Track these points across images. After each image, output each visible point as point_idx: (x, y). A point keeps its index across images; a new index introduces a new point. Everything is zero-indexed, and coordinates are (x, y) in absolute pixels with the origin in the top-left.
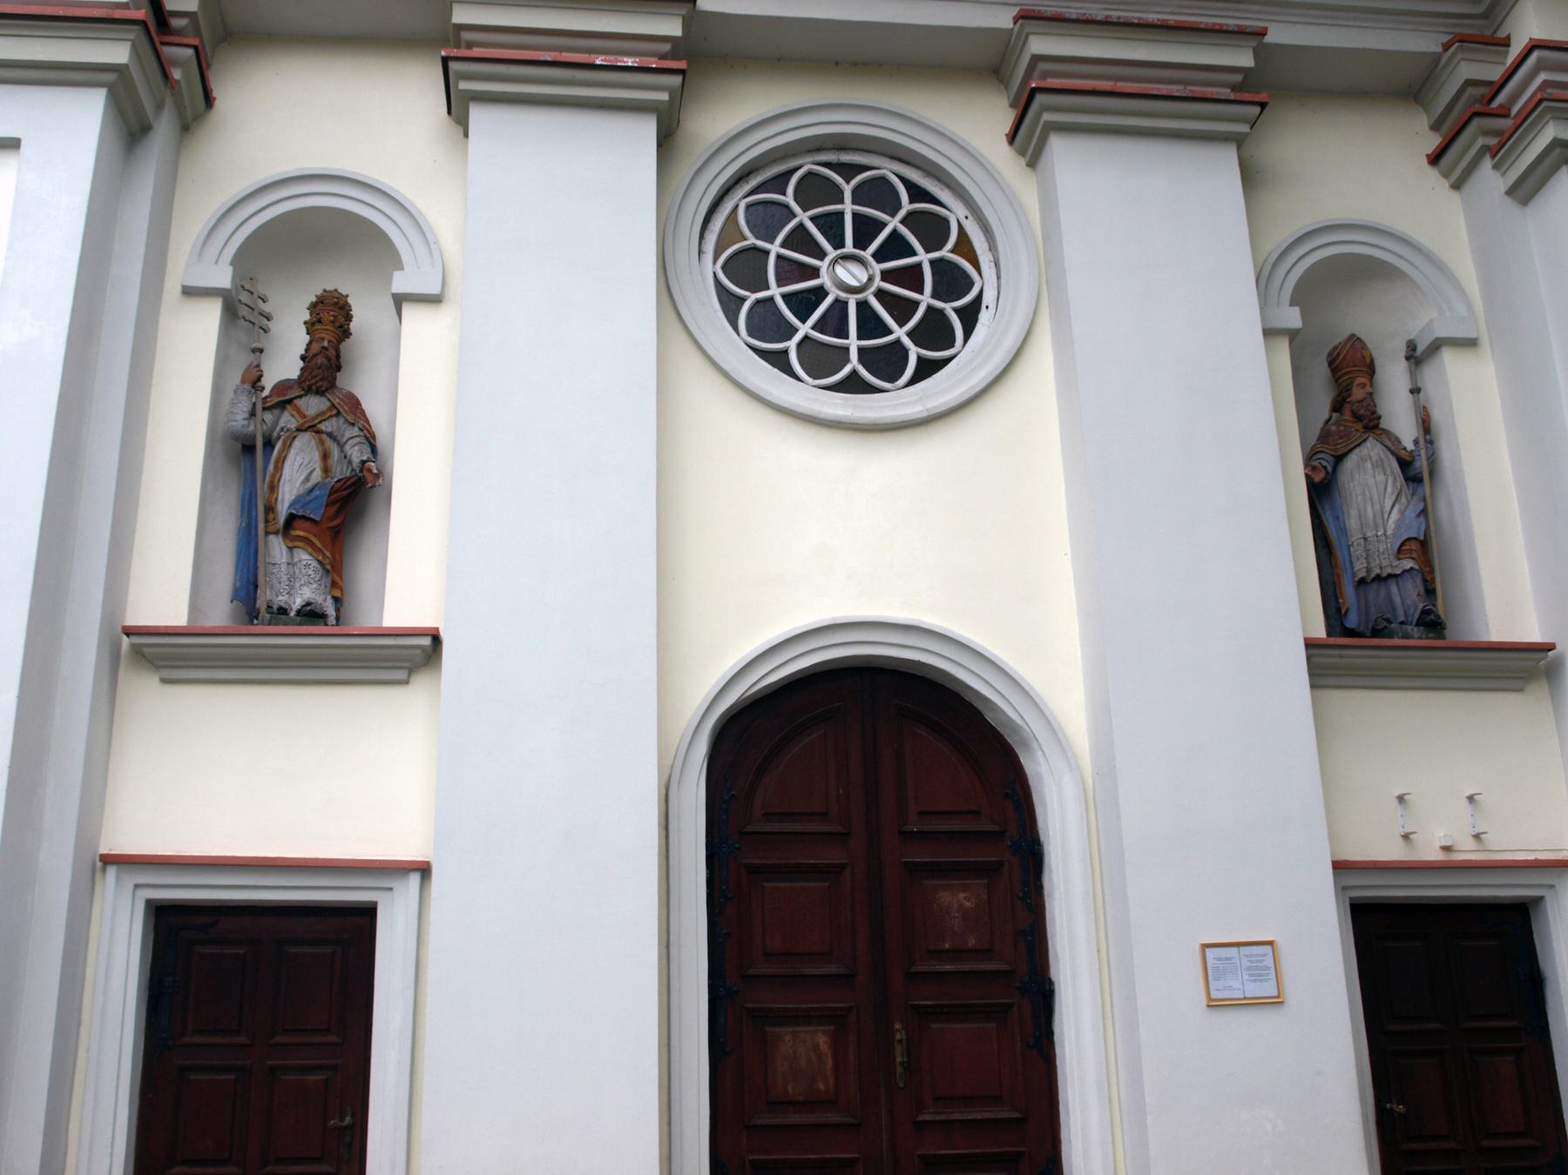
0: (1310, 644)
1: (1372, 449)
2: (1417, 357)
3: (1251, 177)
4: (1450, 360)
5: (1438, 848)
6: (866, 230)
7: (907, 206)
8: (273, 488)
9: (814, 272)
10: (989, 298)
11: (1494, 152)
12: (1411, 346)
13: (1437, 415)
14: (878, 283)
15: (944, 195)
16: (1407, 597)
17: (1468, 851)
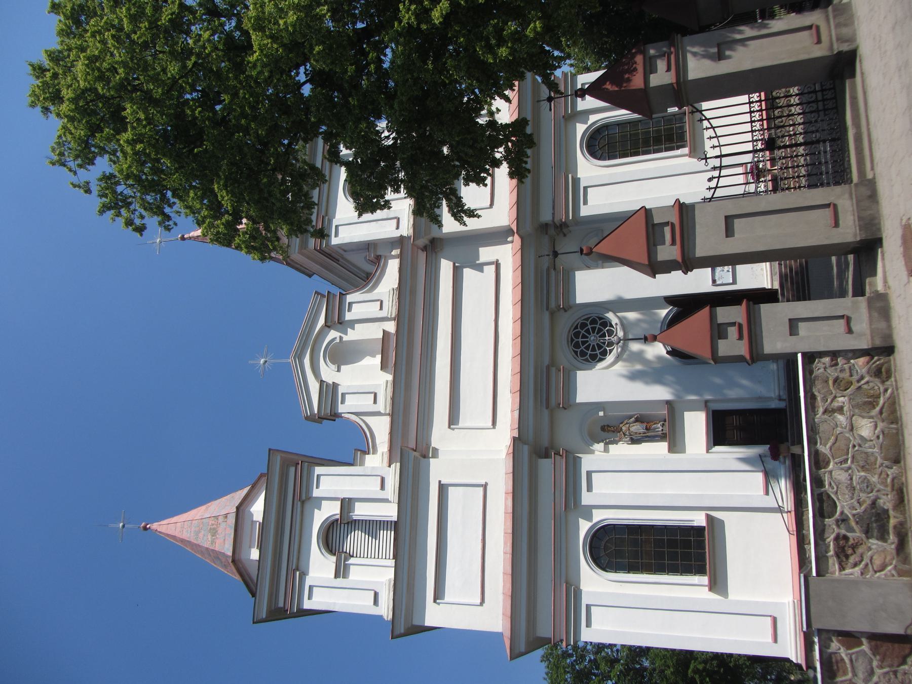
7: (579, 329)
10: (597, 315)
14: (590, 342)
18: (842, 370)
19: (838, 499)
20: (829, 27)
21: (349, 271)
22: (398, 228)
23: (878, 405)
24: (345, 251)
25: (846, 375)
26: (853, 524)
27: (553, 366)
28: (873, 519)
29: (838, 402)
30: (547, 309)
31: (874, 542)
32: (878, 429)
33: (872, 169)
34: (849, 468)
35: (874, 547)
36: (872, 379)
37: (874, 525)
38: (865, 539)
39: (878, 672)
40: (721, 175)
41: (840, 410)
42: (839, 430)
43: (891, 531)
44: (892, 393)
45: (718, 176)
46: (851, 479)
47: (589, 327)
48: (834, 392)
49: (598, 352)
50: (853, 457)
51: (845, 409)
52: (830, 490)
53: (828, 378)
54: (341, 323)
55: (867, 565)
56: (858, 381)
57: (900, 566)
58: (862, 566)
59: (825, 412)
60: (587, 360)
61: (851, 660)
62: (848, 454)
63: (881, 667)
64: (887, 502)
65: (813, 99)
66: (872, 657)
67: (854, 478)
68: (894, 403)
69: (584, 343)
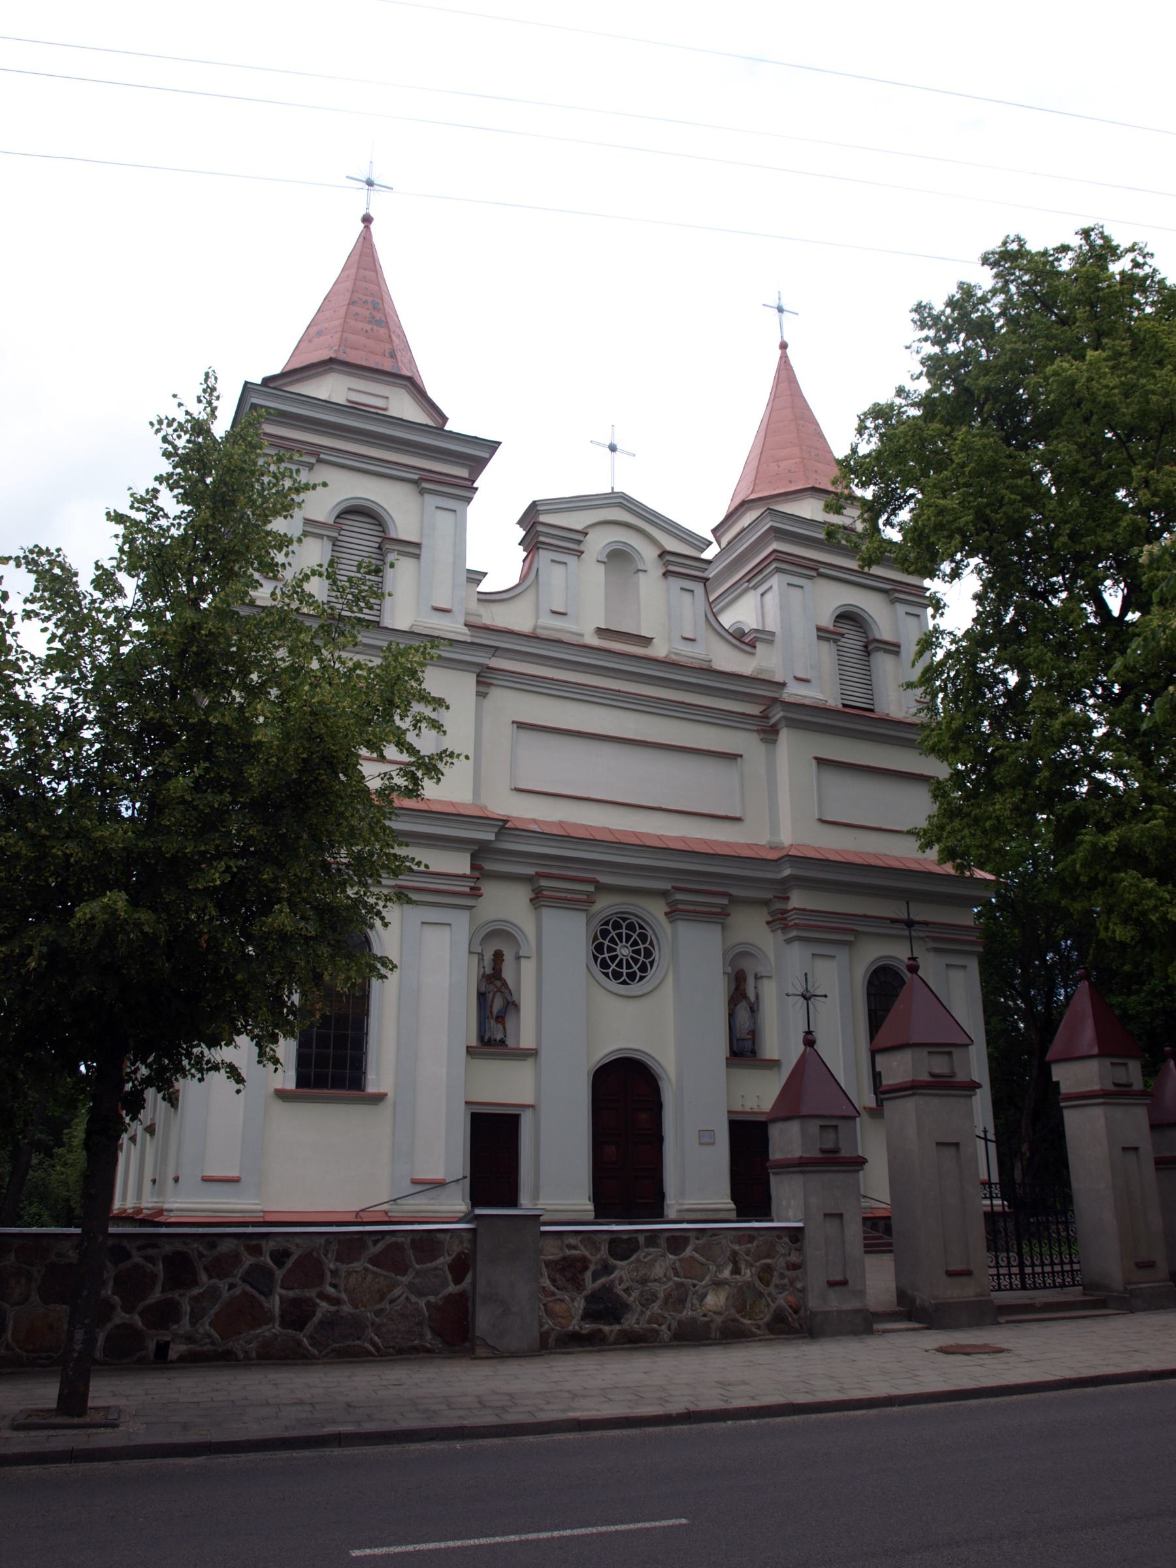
0: (727, 1058)
1: (744, 1004)
2: (757, 977)
3: (613, 488)
4: (765, 982)
5: (272, 1090)
6: (635, 943)
7: (638, 931)
8: (491, 1007)
9: (615, 950)
10: (657, 959)
11: (783, 929)
12: (756, 975)
13: (760, 994)
14: (620, 944)
15: (647, 928)
16: (749, 1045)
17: (756, 1109)
18: (782, 1276)
19: (631, 1263)
20: (1159, 1281)
21: (726, 590)
22: (797, 679)
23: (742, 1316)
24: (762, 595)
25: (776, 1280)
26: (603, 1280)
27: (730, 901)
28: (610, 1305)
29: (746, 1268)
30: (775, 897)
31: (580, 1304)
32: (715, 1316)
33: (1008, 1322)
34: (669, 1279)
35: (576, 1304)
36: (772, 1310)
37: (602, 1306)
38: (585, 1293)
39: (422, 1303)
40: (989, 1143)
41: (736, 1271)
42: (713, 1268)
43: (595, 1326)
44: (755, 1335)
45: (983, 1142)
46: (655, 1280)
47: (642, 946)
48: (757, 1264)
49: (606, 955)
50: (682, 1284)
51: (738, 1277)
52: (643, 1254)
53: (773, 1257)
54: (664, 574)
55: (553, 1294)
56: (769, 1294)
57: (553, 1335)
58: (553, 1288)
59: (735, 1254)
60: (595, 938)
61: (436, 1269)
62: (686, 1278)
63: (428, 1304)
64: (630, 1322)
65: (1000, 1261)
66: (441, 1296)
67: (657, 1284)
68: (745, 1336)
69: (620, 935)
